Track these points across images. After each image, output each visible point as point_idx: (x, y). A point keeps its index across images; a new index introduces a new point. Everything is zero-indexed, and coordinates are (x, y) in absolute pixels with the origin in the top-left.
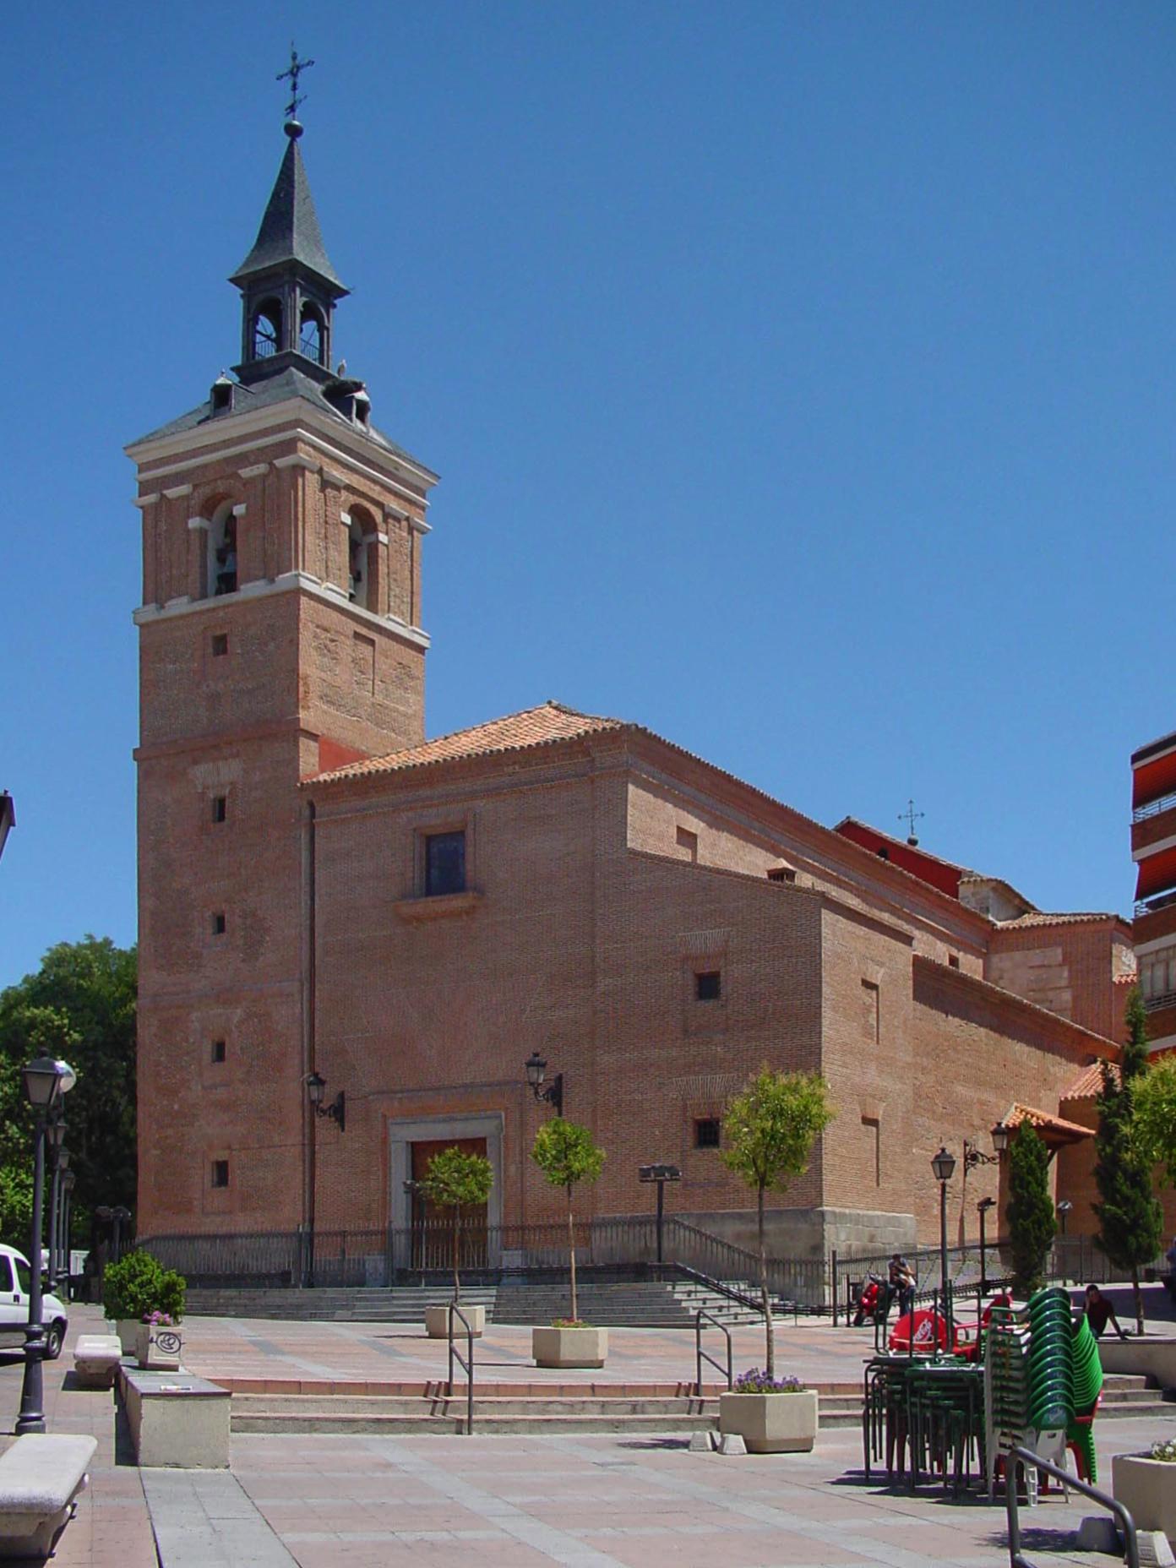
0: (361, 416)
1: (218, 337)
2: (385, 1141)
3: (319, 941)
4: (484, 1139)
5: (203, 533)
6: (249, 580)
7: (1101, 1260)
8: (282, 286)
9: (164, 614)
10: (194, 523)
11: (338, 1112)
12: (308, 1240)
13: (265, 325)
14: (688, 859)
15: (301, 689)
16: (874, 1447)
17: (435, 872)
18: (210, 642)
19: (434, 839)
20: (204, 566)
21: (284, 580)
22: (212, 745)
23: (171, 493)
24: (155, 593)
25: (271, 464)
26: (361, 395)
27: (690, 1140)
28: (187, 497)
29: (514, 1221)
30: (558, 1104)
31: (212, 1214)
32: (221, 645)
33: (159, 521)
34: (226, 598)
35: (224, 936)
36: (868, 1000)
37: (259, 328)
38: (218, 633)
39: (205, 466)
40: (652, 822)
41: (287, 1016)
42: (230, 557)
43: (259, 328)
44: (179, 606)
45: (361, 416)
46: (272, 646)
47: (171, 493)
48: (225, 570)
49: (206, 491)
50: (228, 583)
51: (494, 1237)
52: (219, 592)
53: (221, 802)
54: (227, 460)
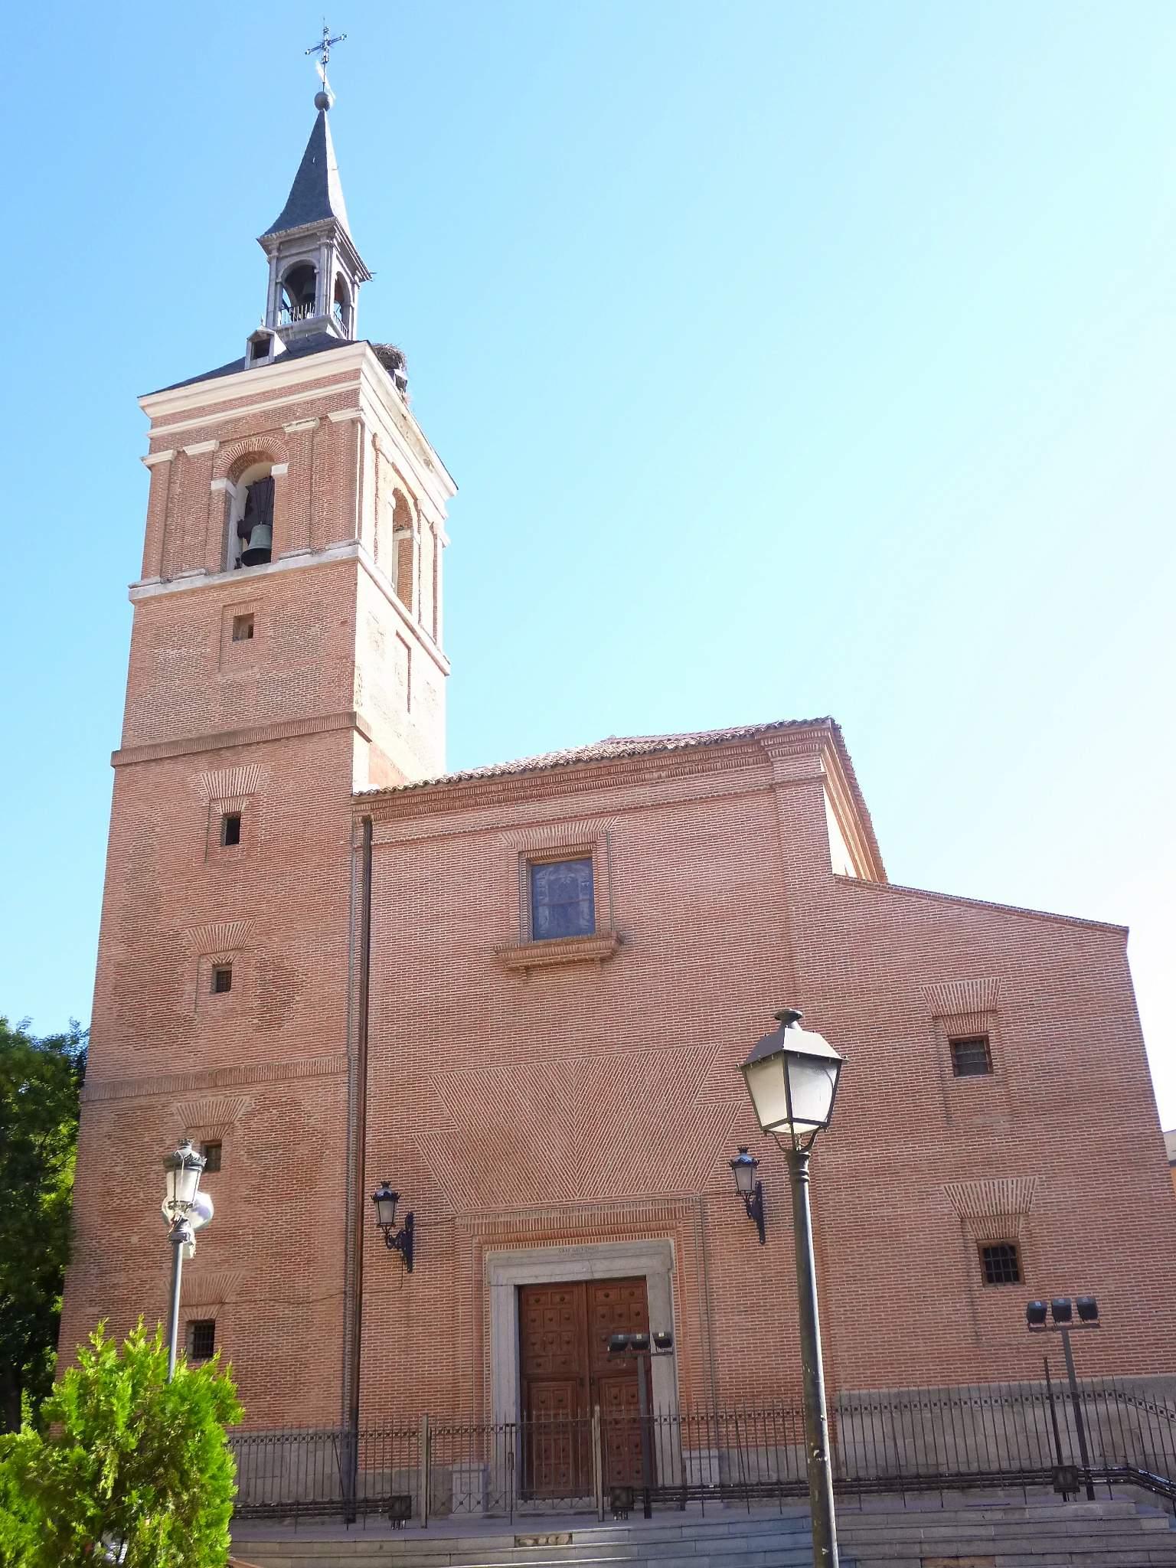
1: (249, 295)
2: (480, 1287)
3: (374, 1002)
5: (228, 498)
8: (319, 249)
9: (172, 587)
11: (404, 1244)
12: (350, 1438)
17: (544, 912)
19: (562, 850)
20: (225, 536)
23: (192, 450)
27: (977, 1276)
28: (213, 455)
33: (172, 483)
35: (228, 997)
38: (242, 611)
39: (238, 420)
41: (324, 1104)
46: (316, 629)
47: (192, 450)
49: (236, 449)
51: (665, 1436)
54: (266, 414)
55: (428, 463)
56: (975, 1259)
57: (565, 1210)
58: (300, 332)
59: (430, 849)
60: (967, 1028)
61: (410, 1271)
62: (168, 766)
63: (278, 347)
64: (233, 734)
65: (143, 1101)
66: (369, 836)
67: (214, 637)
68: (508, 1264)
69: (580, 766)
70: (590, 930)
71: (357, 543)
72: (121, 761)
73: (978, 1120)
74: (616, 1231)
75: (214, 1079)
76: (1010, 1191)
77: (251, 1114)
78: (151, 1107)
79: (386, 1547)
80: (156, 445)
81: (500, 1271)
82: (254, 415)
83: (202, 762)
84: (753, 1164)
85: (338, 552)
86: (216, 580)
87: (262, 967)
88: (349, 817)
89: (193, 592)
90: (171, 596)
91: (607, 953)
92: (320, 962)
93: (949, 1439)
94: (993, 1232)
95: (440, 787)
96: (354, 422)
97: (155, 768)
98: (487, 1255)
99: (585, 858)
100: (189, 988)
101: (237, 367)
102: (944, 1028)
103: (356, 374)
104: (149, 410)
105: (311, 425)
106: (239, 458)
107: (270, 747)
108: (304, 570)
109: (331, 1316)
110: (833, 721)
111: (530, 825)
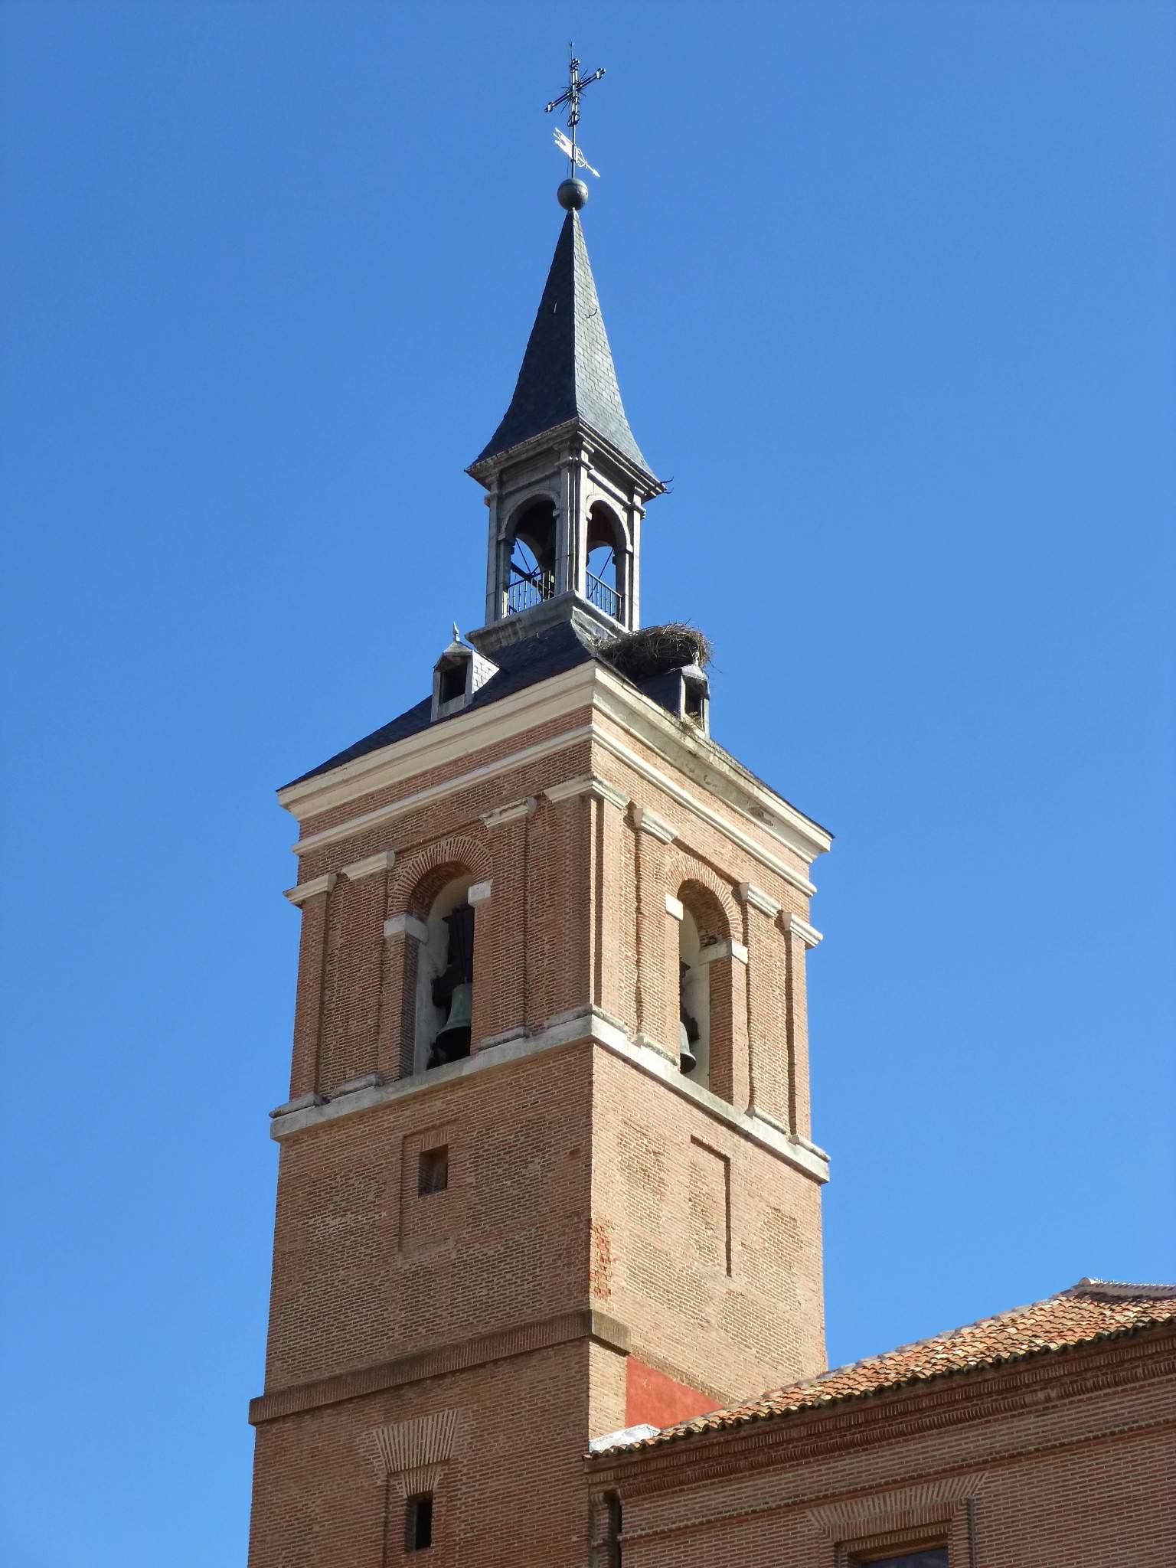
0: (694, 706)
1: (451, 582)
5: (411, 945)
6: (494, 1028)
8: (558, 473)
9: (331, 1111)
10: (395, 927)
13: (524, 556)
15: (594, 1253)
16: (590, 623)
18: (415, 1163)
21: (561, 1031)
22: (401, 1382)
23: (356, 871)
24: (315, 1076)
25: (540, 797)
26: (693, 670)
28: (387, 875)
32: (434, 1169)
33: (331, 924)
34: (449, 1072)
37: (516, 559)
38: (431, 1144)
39: (418, 813)
42: (458, 995)
43: (516, 559)
46: (535, 1166)
47: (356, 871)
48: (452, 1023)
49: (420, 861)
50: (454, 1045)
52: (434, 1063)
53: (422, 1508)
54: (460, 799)
55: (760, 812)
58: (534, 625)
62: (327, 1419)
63: (483, 671)
64: (418, 1359)
66: (616, 1525)
67: (393, 1190)
72: (265, 1414)
85: (561, 1031)
86: (392, 1094)
88: (583, 1494)
89: (362, 1115)
90: (332, 1124)
95: (714, 1438)
96: (584, 799)
97: (311, 1425)
101: (415, 721)
103: (584, 716)
104: (296, 809)
105: (521, 811)
106: (425, 877)
108: (517, 1066)
111: (854, 1494)
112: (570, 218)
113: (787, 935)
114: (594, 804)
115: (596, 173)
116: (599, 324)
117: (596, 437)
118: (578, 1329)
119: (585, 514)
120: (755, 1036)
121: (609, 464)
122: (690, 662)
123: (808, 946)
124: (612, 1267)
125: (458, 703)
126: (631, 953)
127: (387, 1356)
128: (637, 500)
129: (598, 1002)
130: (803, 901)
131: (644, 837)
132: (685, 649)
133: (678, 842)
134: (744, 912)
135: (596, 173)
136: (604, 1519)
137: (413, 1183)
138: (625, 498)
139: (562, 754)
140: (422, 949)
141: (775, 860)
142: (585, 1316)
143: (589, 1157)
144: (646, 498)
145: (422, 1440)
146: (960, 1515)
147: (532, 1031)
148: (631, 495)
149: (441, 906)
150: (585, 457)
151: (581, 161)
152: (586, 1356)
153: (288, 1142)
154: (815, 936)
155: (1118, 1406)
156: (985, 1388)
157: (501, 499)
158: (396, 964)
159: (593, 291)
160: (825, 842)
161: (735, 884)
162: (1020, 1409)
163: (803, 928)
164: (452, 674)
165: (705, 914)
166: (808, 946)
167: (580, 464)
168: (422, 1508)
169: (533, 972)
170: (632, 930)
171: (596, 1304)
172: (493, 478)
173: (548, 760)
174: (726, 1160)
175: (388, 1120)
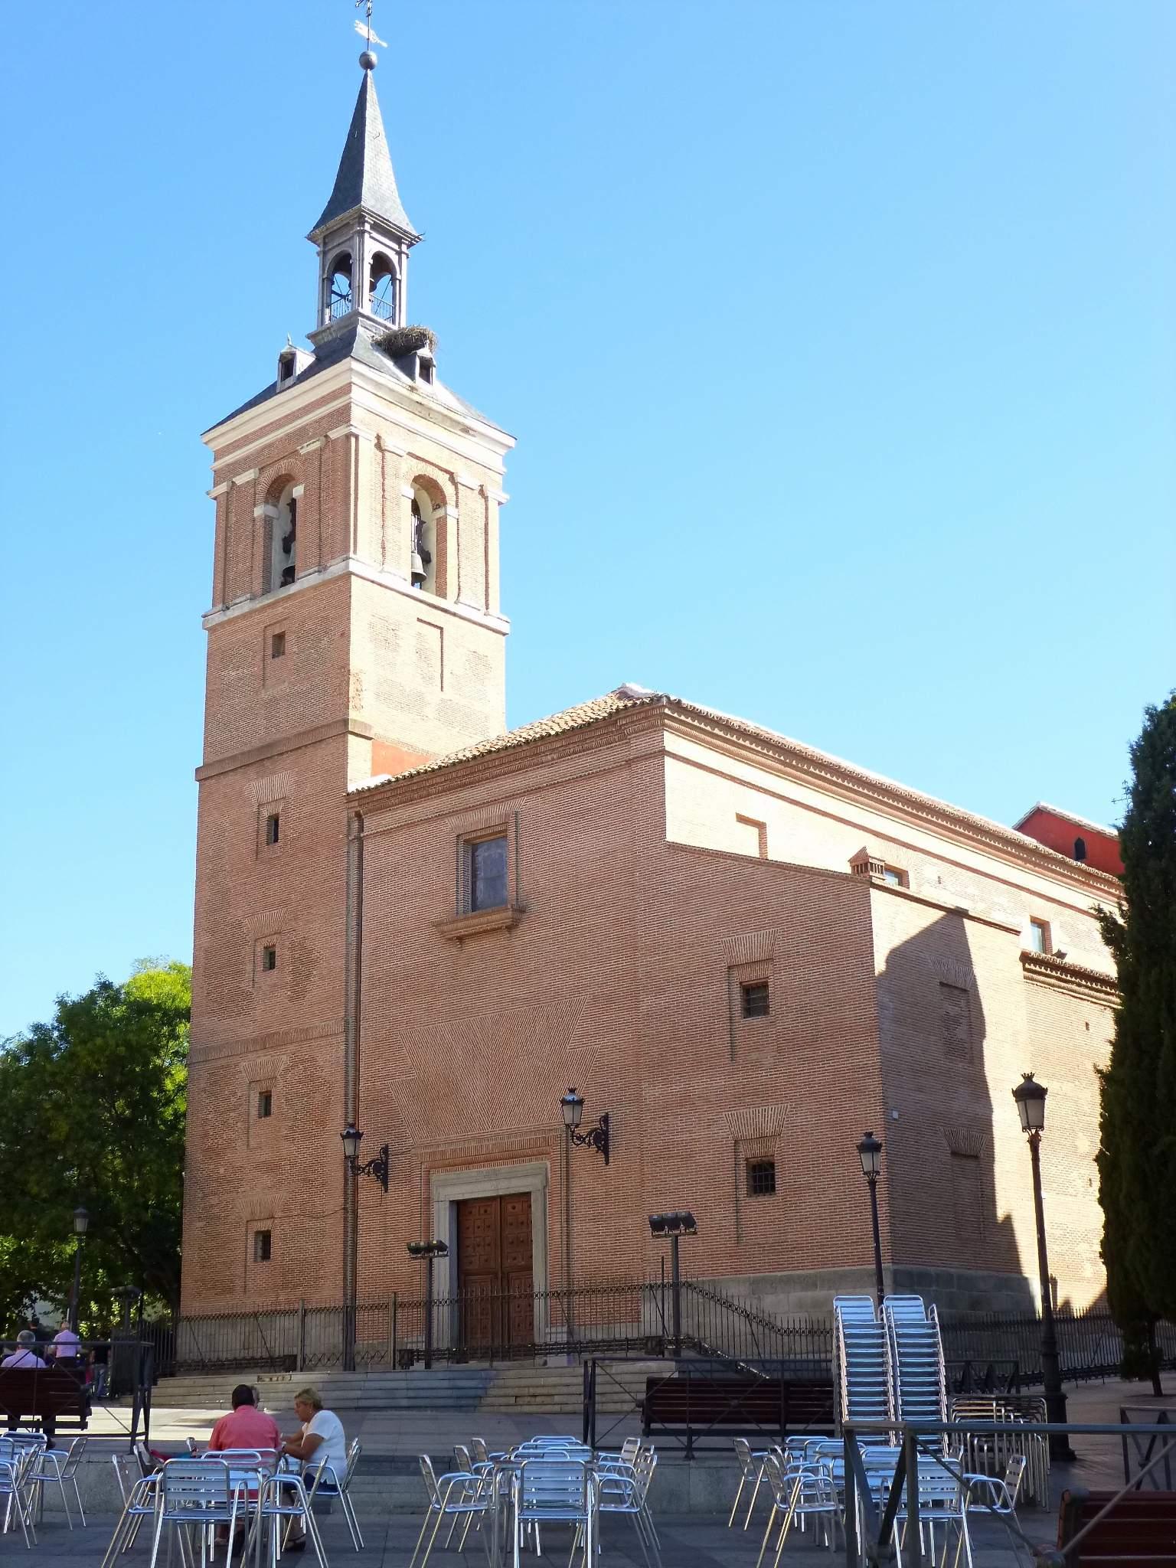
0: (426, 374)
2: (428, 1202)
4: (529, 1194)
5: (268, 521)
7: (291, 1544)
8: (352, 238)
10: (258, 511)
11: (381, 1169)
14: (753, 852)
18: (270, 641)
21: (335, 569)
23: (240, 480)
24: (223, 597)
25: (326, 436)
26: (424, 352)
27: (743, 1189)
28: (255, 483)
29: (561, 1286)
30: (605, 1151)
31: (257, 1288)
33: (229, 506)
34: (293, 589)
36: (953, 1010)
37: (335, 288)
39: (270, 445)
40: (704, 805)
41: (330, 1057)
43: (335, 288)
44: (242, 607)
45: (426, 374)
47: (240, 480)
49: (271, 474)
50: (289, 575)
52: (284, 584)
53: (274, 820)
54: (288, 437)
55: (466, 430)
56: (743, 1173)
57: (479, 1140)
58: (340, 328)
59: (400, 837)
60: (751, 976)
61: (607, 1163)
62: (231, 778)
63: (304, 360)
64: (270, 746)
65: (223, 1062)
66: (361, 829)
67: (259, 657)
68: (445, 1184)
69: (494, 756)
70: (500, 903)
71: (348, 558)
72: (203, 776)
73: (754, 1056)
74: (512, 1156)
75: (266, 1042)
76: (768, 1117)
77: (287, 1070)
78: (228, 1066)
79: (512, 1400)
80: (219, 476)
81: (440, 1190)
82: (281, 440)
83: (251, 772)
84: (580, 1102)
85: (335, 569)
86: (258, 604)
87: (292, 949)
88: (345, 813)
89: (244, 616)
90: (230, 622)
91: (509, 922)
92: (326, 938)
93: (719, 1320)
94: (757, 1151)
95: (402, 783)
96: (348, 436)
97: (224, 780)
98: (434, 1178)
99: (498, 836)
100: (249, 967)
101: (270, 392)
102: (737, 976)
103: (346, 389)
104: (212, 445)
105: (317, 445)
106: (274, 482)
107: (293, 756)
108: (315, 588)
109: (334, 1226)
110: (668, 698)
111: (467, 810)
112: (366, 76)
113: (486, 498)
114: (353, 440)
115: (385, 45)
116: (383, 142)
117: (372, 214)
118: (341, 728)
119: (368, 260)
120: (462, 559)
121: (383, 228)
122: (423, 346)
123: (500, 503)
124: (363, 694)
125: (290, 381)
126: (379, 522)
127: (257, 744)
128: (404, 248)
129: (355, 552)
130: (499, 478)
131: (387, 454)
132: (421, 340)
133: (409, 454)
134: (456, 489)
135: (385, 45)
136: (355, 825)
137: (270, 652)
138: (396, 247)
139: (337, 411)
140: (275, 522)
141: (476, 460)
142: (346, 722)
143: (349, 636)
144: (409, 247)
145: (272, 787)
146: (512, 820)
147: (322, 568)
148: (400, 244)
149: (283, 501)
150: (367, 227)
151: (374, 38)
152: (346, 742)
153: (212, 630)
154: (504, 497)
155: (585, 762)
156: (523, 755)
157: (324, 253)
158: (260, 532)
159: (380, 120)
160: (511, 442)
161: (451, 474)
162: (540, 764)
163: (496, 493)
164: (287, 364)
165: (429, 494)
166: (500, 503)
167: (364, 232)
168: (274, 820)
169: (324, 535)
170: (379, 508)
171: (353, 715)
172: (320, 241)
173: (331, 415)
174: (441, 629)
175: (256, 618)
